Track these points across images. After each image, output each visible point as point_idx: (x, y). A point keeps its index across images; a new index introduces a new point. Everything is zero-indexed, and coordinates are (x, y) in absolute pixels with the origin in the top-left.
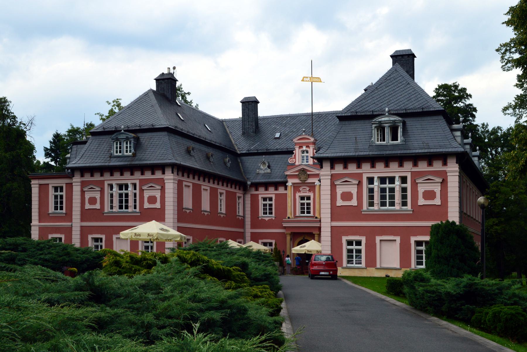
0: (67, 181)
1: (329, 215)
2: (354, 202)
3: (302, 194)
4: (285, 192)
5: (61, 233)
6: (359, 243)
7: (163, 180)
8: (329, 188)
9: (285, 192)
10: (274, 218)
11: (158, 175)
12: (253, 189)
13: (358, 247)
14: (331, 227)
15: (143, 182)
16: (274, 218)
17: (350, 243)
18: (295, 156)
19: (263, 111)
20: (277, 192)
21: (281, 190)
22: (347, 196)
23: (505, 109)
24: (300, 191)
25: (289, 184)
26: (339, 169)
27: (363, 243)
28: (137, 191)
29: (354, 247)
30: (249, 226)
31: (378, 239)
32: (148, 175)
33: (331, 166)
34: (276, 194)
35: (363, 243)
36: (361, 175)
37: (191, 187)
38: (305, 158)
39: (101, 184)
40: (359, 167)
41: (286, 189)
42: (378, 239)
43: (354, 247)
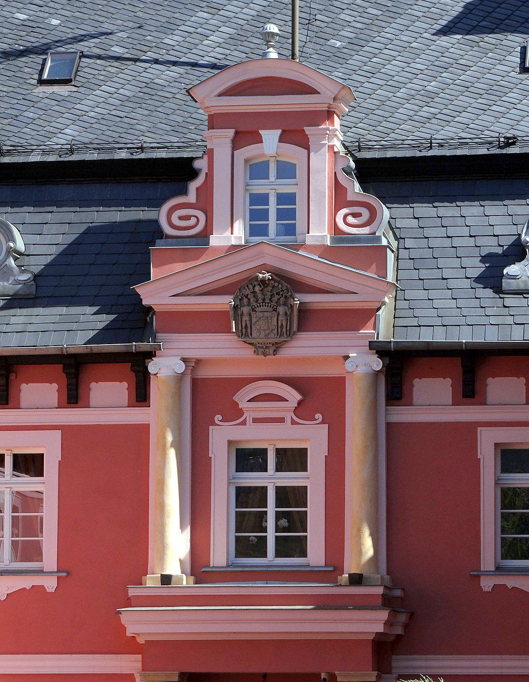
3: (253, 436)
4: (136, 416)
9: (136, 416)
10: (50, 584)
16: (50, 584)
18: (206, 192)
21: (107, 403)
24: (234, 414)
25: (164, 367)
34: (69, 433)
41: (141, 395)
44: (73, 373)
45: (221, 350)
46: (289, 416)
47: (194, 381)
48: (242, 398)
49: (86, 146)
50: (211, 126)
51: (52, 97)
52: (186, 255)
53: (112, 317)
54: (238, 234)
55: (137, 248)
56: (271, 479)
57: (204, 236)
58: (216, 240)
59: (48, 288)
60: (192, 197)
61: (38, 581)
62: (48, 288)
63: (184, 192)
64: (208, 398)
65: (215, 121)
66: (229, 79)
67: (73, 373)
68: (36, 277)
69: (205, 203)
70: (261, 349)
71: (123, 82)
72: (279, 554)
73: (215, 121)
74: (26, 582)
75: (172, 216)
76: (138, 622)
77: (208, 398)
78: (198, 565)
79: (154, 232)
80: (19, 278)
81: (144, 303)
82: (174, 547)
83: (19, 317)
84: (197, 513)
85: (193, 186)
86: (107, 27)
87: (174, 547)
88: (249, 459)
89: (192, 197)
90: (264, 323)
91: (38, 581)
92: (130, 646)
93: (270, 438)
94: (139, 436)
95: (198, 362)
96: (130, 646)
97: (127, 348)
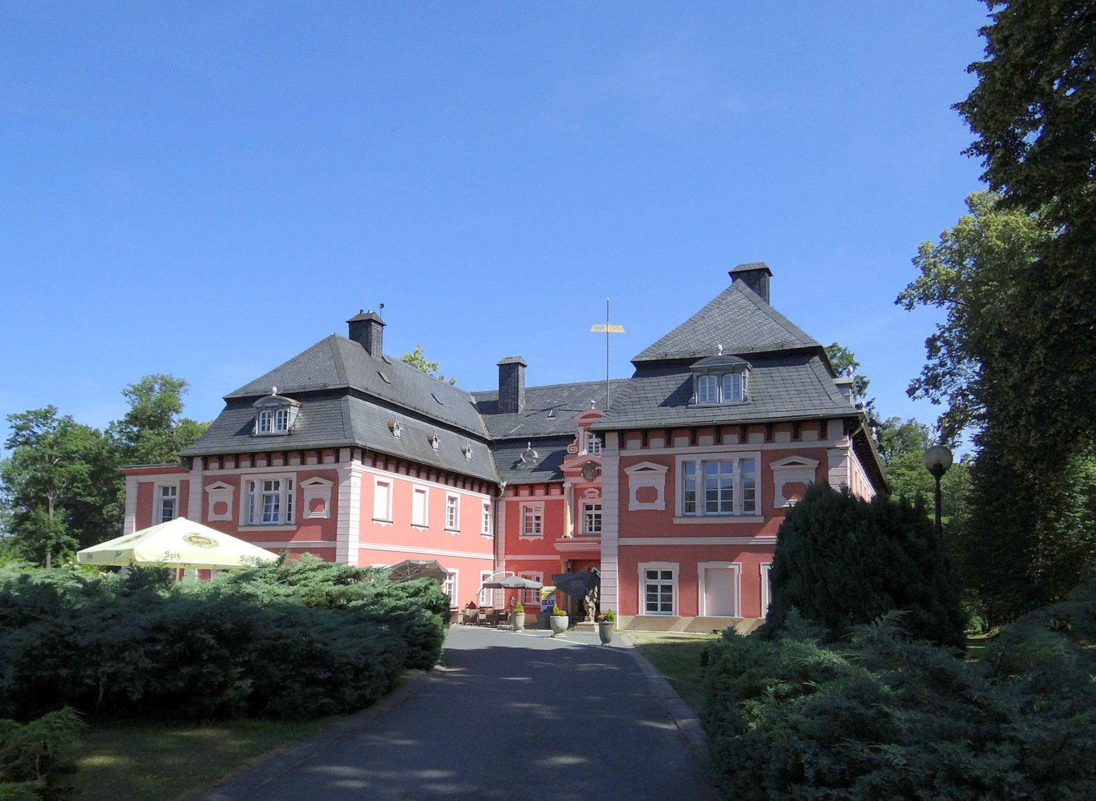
0: (183, 476)
1: (616, 528)
2: (660, 504)
3: (589, 502)
4: (561, 497)
5: (456, 568)
6: (667, 575)
7: (335, 471)
8: (616, 481)
9: (561, 497)
10: (542, 538)
11: (329, 464)
12: (511, 493)
13: (667, 582)
14: (619, 546)
15: (303, 476)
16: (542, 538)
17: (652, 575)
18: (578, 442)
19: (529, 379)
20: (547, 498)
21: (555, 494)
22: (647, 494)
23: (911, 392)
24: (584, 496)
25: (567, 485)
26: (634, 447)
27: (675, 575)
28: (293, 492)
29: (659, 582)
30: (357, 538)
31: (702, 566)
32: (312, 464)
33: (619, 443)
34: (546, 501)
35: (675, 575)
36: (673, 456)
37: (391, 486)
38: (594, 445)
39: (234, 481)
40: (669, 443)
41: (562, 493)
42: (702, 566)
43: (659, 582)
44: (547, 487)
45: (579, 480)
46: (597, 497)
47: (575, 489)
48: (586, 492)
49: (554, 432)
50: (579, 426)
51: (550, 420)
52: (572, 458)
53: (839, 491)
54: (585, 452)
55: (559, 458)
56: (593, 512)
57: (577, 453)
58: (579, 454)
59: (542, 467)
60: (575, 444)
61: (539, 537)
62: (542, 467)
63: (573, 443)
64: (578, 492)
65: (580, 425)
66: (582, 414)
67: (547, 487)
68: (540, 464)
69: (577, 445)
70: (588, 480)
71: (567, 416)
72: (595, 530)
73: (580, 425)
74: (537, 538)
75: (570, 448)
76: (558, 547)
77: (578, 492)
78: (575, 533)
79: (565, 452)
80: (536, 464)
81: (874, 494)
82: (569, 528)
83: (535, 474)
84: (575, 520)
85: (575, 441)
86: (381, 360)
87: (569, 528)
88: (589, 508)
89: (575, 444)
90: (589, 474)
91: (539, 537)
92: (557, 553)
93: (593, 502)
94: (561, 503)
95: (575, 484)
96: (557, 553)
97: (557, 483)
